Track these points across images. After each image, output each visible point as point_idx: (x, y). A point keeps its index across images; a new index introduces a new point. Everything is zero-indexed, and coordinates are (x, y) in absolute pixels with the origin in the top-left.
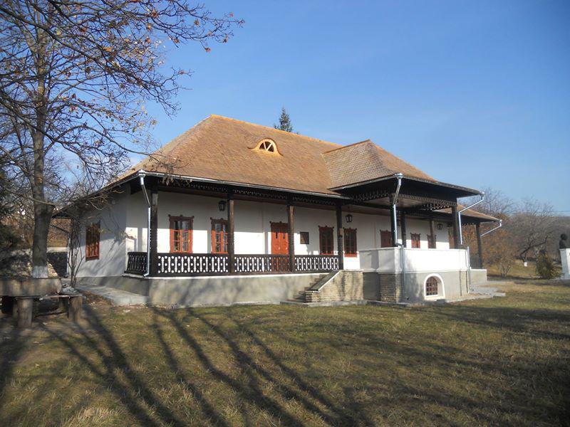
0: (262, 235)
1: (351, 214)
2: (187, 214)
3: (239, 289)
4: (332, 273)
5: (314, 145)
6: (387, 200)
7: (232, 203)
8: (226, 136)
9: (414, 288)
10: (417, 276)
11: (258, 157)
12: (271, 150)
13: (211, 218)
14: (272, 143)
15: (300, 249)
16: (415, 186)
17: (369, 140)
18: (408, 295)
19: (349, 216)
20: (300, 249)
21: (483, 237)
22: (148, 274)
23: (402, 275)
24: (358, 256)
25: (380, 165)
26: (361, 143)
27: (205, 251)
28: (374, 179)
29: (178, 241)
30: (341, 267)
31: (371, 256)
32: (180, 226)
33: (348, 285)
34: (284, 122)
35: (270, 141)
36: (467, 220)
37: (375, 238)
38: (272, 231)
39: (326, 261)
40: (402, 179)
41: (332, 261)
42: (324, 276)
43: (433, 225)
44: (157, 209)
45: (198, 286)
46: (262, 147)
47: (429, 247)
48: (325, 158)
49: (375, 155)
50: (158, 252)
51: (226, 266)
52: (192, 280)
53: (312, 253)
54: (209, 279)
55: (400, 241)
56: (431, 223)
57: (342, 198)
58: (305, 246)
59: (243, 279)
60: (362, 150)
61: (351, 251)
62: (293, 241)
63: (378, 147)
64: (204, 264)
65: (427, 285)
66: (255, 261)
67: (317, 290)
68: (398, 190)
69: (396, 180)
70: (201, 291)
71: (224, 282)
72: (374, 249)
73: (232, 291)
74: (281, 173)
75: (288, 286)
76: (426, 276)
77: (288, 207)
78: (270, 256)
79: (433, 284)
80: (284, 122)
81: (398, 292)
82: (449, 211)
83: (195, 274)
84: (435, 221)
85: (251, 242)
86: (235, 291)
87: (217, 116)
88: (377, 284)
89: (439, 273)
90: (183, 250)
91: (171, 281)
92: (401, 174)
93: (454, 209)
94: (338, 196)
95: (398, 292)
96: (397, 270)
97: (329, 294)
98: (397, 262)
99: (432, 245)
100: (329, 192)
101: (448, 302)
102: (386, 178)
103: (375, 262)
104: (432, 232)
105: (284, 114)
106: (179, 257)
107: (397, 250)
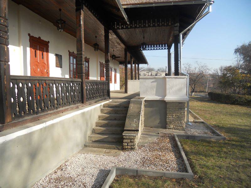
31: (155, 84)
38: (31, 47)
53: (65, 76)
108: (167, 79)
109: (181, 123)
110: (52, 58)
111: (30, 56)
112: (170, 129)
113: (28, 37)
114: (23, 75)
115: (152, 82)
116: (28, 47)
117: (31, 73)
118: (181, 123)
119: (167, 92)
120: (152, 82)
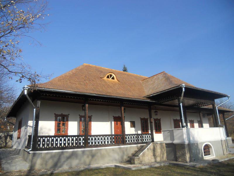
0: (109, 123)
1: (157, 111)
2: (65, 113)
3: (93, 156)
4: (148, 143)
5: (136, 77)
6: (176, 102)
7: (87, 105)
8: (90, 72)
9: (198, 151)
10: (198, 144)
11: (105, 82)
12: (113, 78)
13: (79, 115)
14: (113, 75)
15: (129, 129)
16: (191, 92)
17: (164, 72)
18: (195, 157)
19: (156, 112)
20: (129, 129)
21: (226, 120)
22: (31, 149)
23: (189, 144)
24: (162, 132)
25: (171, 82)
26: (160, 73)
27: (76, 134)
28: (168, 89)
29: (60, 128)
30: (153, 141)
31: (169, 133)
32: (62, 121)
33: (158, 151)
34: (125, 70)
35: (112, 74)
36: (222, 112)
37: (171, 126)
38: (114, 121)
39: (146, 138)
40: (185, 88)
41: (147, 137)
42: (142, 146)
43: (201, 115)
44: (39, 110)
45: (67, 155)
46: (108, 77)
47: (199, 127)
48: (143, 83)
49: (168, 78)
50: (38, 135)
51: (83, 143)
52: (62, 152)
53: (137, 132)
54: (73, 152)
55: (185, 124)
56: (200, 115)
57: (151, 101)
58: (133, 128)
59: (96, 150)
60: (160, 76)
61: (158, 130)
62: (124, 127)
63: (169, 75)
64: (69, 142)
65: (204, 149)
66: (101, 139)
67: (138, 156)
68: (183, 94)
69: (181, 89)
70: (69, 158)
71: (83, 152)
72: (171, 129)
73: (88, 157)
74: (117, 90)
75: (123, 153)
76: (203, 144)
77: (121, 107)
78: (113, 135)
79: (207, 149)
80: (125, 70)
81: (188, 156)
82: (210, 107)
83: (63, 148)
84: (202, 113)
85: (101, 128)
86: (90, 157)
87: (87, 64)
88: (175, 149)
89: (210, 142)
90: (63, 133)
91: (47, 153)
92: (184, 85)
93: (213, 105)
94: (149, 100)
95: (188, 156)
96: (187, 142)
97: (147, 157)
98: (185, 136)
99: (201, 126)
100: (143, 98)
101: (220, 161)
102: (175, 88)
103: (172, 138)
104: (201, 118)
105: (124, 67)
106: (65, 138)
107: (184, 130)
108: (174, 131)
109: (184, 158)
110: (127, 124)
111: (54, 125)
112: (179, 161)
113: (113, 117)
114: (110, 134)
115: (168, 133)
116: (196, 123)
117: (115, 132)
118: (184, 158)
119: (175, 138)
120: (168, 133)
